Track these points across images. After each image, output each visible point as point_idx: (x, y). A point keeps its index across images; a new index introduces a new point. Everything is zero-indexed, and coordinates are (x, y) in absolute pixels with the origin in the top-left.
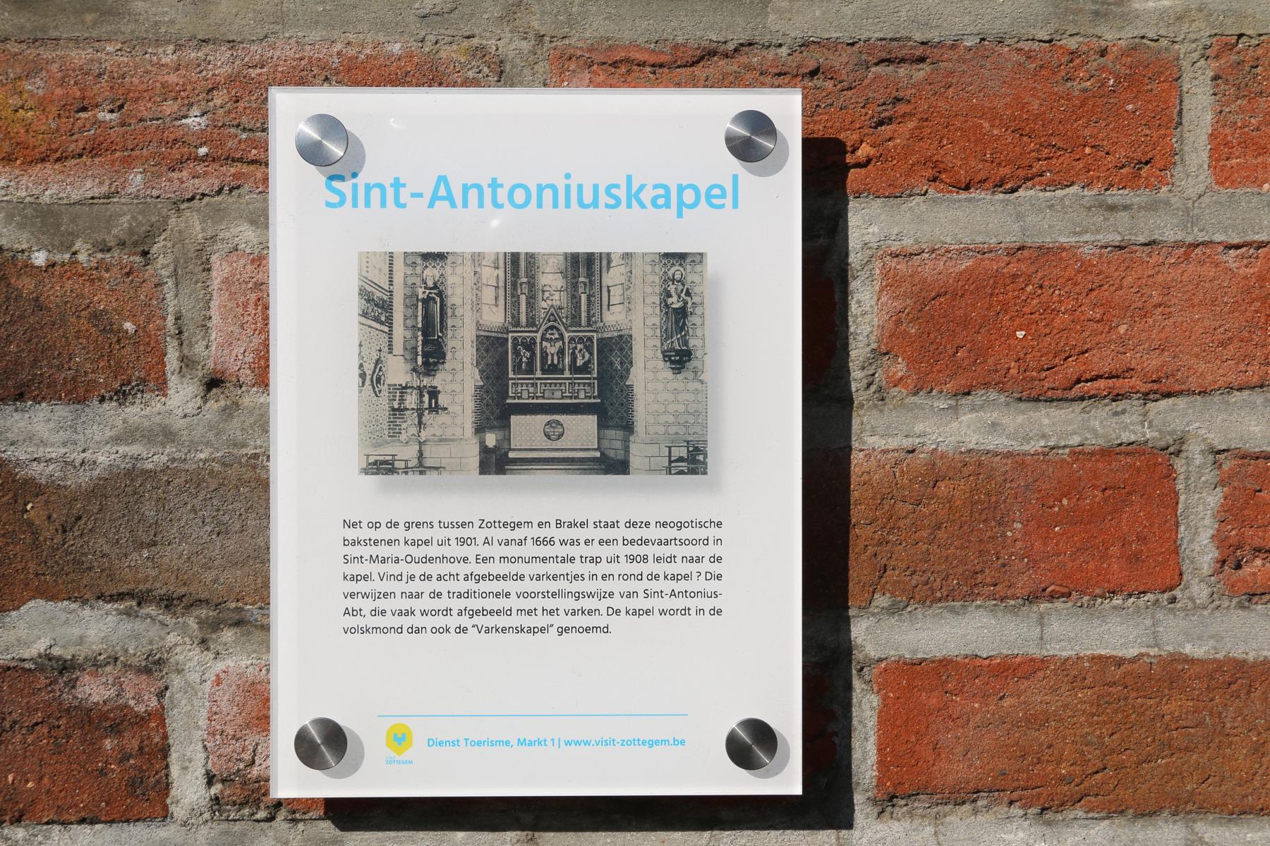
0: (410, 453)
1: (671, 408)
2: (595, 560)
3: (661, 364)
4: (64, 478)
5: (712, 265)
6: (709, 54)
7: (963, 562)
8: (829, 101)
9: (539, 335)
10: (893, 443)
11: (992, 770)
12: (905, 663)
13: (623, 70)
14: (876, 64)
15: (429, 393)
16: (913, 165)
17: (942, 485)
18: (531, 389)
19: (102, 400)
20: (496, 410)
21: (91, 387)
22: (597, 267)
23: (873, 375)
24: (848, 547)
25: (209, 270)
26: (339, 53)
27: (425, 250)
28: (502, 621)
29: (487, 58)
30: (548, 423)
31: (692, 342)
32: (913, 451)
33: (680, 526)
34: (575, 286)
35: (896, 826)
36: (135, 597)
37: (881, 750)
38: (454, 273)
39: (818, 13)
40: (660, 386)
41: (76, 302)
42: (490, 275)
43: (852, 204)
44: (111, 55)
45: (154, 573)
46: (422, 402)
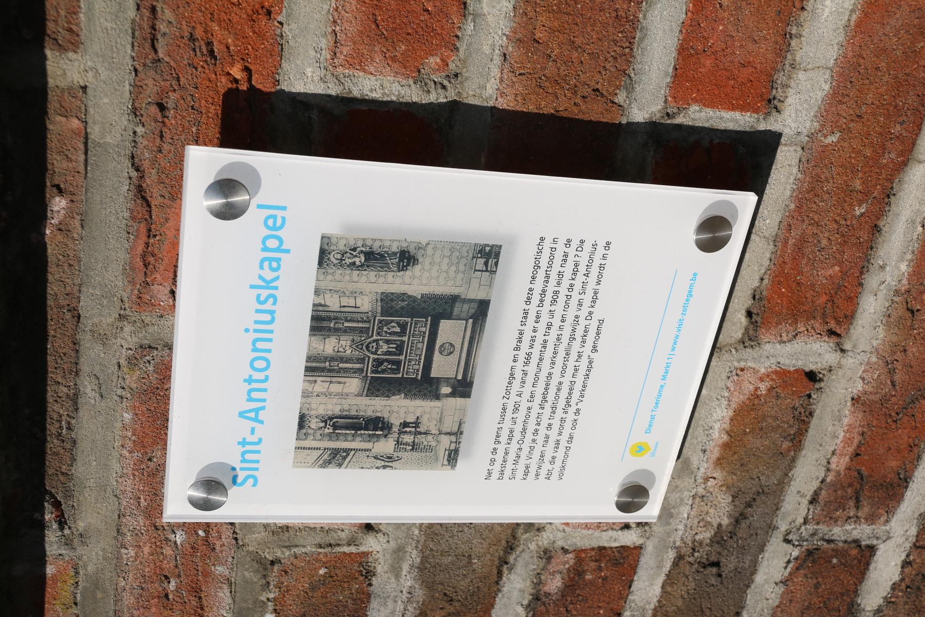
0: (446, 441)
1: (444, 267)
2: (549, 326)
3: (408, 273)
4: (418, 602)
5: (332, 230)
6: (140, 193)
7: (605, 25)
8: (189, 98)
9: (372, 356)
10: (495, 72)
11: (774, 21)
12: (673, 83)
13: (152, 259)
14: (156, 51)
15: (404, 427)
16: (254, 32)
17: (538, 35)
18: (413, 363)
19: (370, 585)
20: (426, 386)
21: (361, 591)
22: (323, 314)
23: (435, 82)
24: (572, 119)
25: (287, 527)
26: (130, 452)
27: (296, 427)
28: (578, 387)
29: (138, 357)
30: (441, 353)
31: (394, 249)
32: (505, 55)
33: (537, 267)
34: (337, 330)
35: (789, 100)
36: (503, 564)
37: (733, 108)
38: (316, 410)
39: (106, 100)
40: (426, 274)
41: (302, 598)
42: (321, 385)
43: (285, 86)
44: (128, 583)
45: (488, 556)
46: (410, 432)
